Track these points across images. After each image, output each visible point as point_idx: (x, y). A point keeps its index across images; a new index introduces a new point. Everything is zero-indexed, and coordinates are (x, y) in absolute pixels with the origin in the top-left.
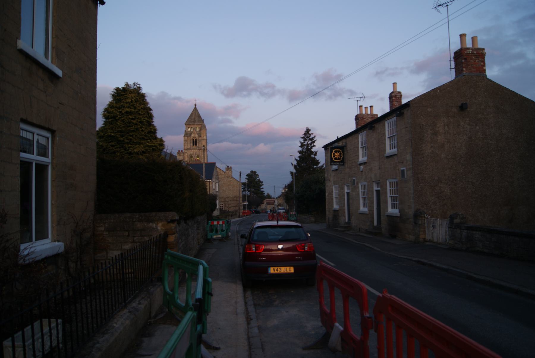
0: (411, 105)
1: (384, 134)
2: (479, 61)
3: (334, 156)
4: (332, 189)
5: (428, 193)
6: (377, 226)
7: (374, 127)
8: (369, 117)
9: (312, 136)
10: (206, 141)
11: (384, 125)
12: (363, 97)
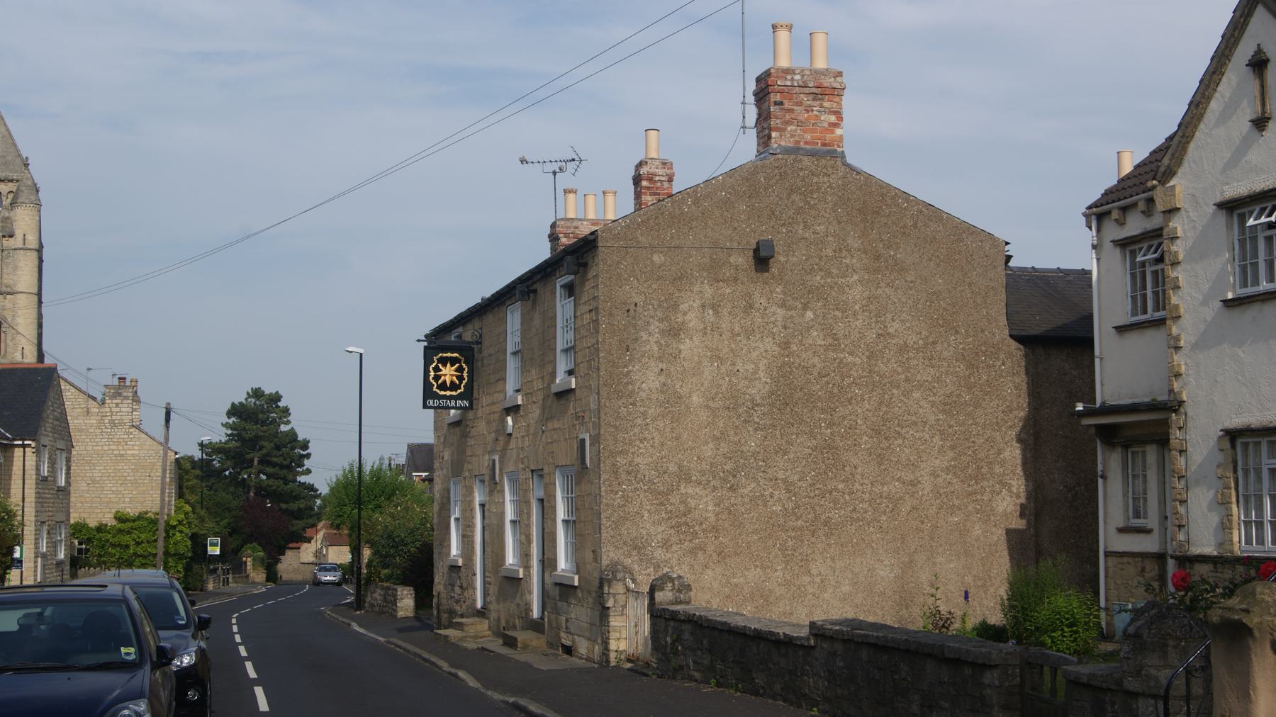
2: (823, 109)
3: (437, 378)
5: (646, 515)
7: (535, 291)
10: (34, 255)
12: (573, 160)
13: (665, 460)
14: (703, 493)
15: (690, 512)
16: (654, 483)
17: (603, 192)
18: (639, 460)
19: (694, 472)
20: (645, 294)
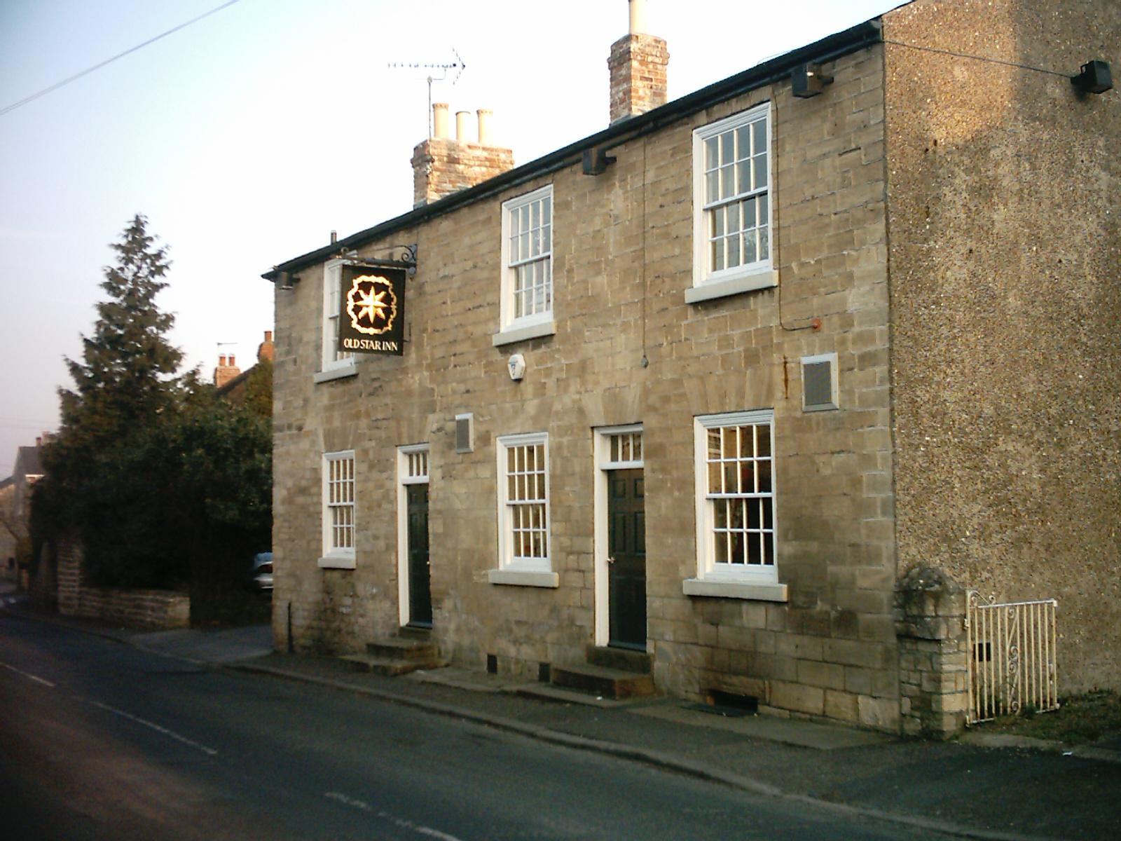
0: (887, 38)
1: (684, 193)
3: (357, 309)
4: (316, 472)
6: (609, 645)
8: (478, 158)
9: (151, 250)
11: (687, 149)
13: (978, 396)
14: (1026, 451)
15: (1011, 481)
16: (966, 434)
17: (478, 112)
18: (946, 394)
19: (1015, 418)
20: (946, 128)
